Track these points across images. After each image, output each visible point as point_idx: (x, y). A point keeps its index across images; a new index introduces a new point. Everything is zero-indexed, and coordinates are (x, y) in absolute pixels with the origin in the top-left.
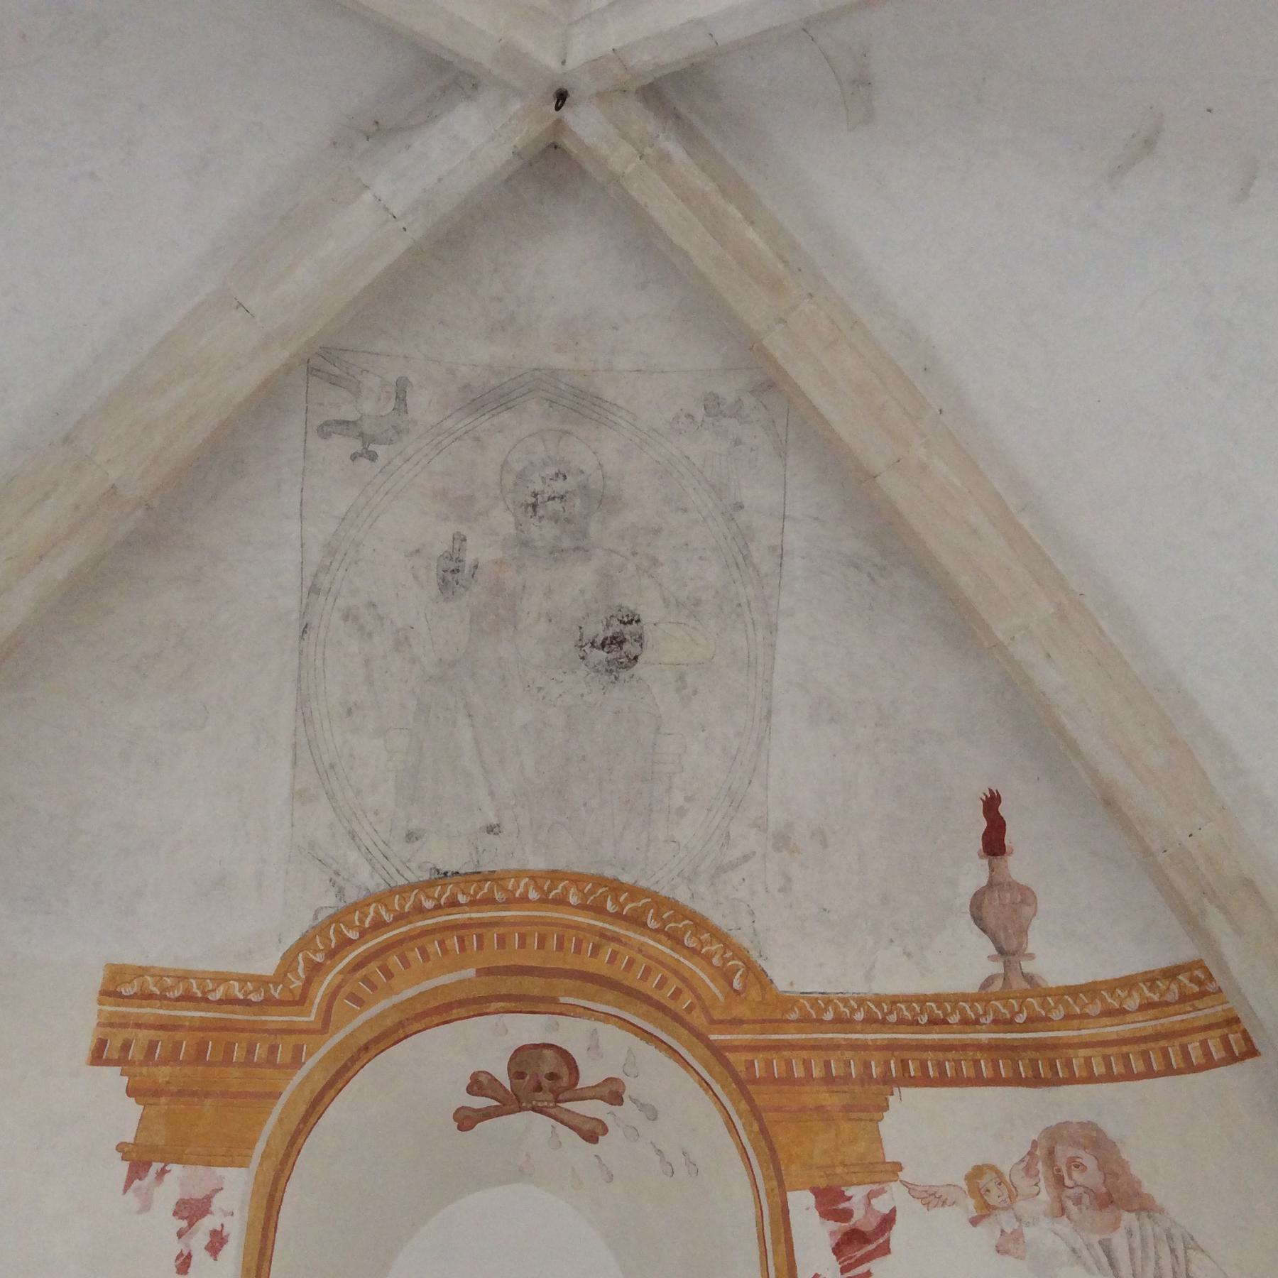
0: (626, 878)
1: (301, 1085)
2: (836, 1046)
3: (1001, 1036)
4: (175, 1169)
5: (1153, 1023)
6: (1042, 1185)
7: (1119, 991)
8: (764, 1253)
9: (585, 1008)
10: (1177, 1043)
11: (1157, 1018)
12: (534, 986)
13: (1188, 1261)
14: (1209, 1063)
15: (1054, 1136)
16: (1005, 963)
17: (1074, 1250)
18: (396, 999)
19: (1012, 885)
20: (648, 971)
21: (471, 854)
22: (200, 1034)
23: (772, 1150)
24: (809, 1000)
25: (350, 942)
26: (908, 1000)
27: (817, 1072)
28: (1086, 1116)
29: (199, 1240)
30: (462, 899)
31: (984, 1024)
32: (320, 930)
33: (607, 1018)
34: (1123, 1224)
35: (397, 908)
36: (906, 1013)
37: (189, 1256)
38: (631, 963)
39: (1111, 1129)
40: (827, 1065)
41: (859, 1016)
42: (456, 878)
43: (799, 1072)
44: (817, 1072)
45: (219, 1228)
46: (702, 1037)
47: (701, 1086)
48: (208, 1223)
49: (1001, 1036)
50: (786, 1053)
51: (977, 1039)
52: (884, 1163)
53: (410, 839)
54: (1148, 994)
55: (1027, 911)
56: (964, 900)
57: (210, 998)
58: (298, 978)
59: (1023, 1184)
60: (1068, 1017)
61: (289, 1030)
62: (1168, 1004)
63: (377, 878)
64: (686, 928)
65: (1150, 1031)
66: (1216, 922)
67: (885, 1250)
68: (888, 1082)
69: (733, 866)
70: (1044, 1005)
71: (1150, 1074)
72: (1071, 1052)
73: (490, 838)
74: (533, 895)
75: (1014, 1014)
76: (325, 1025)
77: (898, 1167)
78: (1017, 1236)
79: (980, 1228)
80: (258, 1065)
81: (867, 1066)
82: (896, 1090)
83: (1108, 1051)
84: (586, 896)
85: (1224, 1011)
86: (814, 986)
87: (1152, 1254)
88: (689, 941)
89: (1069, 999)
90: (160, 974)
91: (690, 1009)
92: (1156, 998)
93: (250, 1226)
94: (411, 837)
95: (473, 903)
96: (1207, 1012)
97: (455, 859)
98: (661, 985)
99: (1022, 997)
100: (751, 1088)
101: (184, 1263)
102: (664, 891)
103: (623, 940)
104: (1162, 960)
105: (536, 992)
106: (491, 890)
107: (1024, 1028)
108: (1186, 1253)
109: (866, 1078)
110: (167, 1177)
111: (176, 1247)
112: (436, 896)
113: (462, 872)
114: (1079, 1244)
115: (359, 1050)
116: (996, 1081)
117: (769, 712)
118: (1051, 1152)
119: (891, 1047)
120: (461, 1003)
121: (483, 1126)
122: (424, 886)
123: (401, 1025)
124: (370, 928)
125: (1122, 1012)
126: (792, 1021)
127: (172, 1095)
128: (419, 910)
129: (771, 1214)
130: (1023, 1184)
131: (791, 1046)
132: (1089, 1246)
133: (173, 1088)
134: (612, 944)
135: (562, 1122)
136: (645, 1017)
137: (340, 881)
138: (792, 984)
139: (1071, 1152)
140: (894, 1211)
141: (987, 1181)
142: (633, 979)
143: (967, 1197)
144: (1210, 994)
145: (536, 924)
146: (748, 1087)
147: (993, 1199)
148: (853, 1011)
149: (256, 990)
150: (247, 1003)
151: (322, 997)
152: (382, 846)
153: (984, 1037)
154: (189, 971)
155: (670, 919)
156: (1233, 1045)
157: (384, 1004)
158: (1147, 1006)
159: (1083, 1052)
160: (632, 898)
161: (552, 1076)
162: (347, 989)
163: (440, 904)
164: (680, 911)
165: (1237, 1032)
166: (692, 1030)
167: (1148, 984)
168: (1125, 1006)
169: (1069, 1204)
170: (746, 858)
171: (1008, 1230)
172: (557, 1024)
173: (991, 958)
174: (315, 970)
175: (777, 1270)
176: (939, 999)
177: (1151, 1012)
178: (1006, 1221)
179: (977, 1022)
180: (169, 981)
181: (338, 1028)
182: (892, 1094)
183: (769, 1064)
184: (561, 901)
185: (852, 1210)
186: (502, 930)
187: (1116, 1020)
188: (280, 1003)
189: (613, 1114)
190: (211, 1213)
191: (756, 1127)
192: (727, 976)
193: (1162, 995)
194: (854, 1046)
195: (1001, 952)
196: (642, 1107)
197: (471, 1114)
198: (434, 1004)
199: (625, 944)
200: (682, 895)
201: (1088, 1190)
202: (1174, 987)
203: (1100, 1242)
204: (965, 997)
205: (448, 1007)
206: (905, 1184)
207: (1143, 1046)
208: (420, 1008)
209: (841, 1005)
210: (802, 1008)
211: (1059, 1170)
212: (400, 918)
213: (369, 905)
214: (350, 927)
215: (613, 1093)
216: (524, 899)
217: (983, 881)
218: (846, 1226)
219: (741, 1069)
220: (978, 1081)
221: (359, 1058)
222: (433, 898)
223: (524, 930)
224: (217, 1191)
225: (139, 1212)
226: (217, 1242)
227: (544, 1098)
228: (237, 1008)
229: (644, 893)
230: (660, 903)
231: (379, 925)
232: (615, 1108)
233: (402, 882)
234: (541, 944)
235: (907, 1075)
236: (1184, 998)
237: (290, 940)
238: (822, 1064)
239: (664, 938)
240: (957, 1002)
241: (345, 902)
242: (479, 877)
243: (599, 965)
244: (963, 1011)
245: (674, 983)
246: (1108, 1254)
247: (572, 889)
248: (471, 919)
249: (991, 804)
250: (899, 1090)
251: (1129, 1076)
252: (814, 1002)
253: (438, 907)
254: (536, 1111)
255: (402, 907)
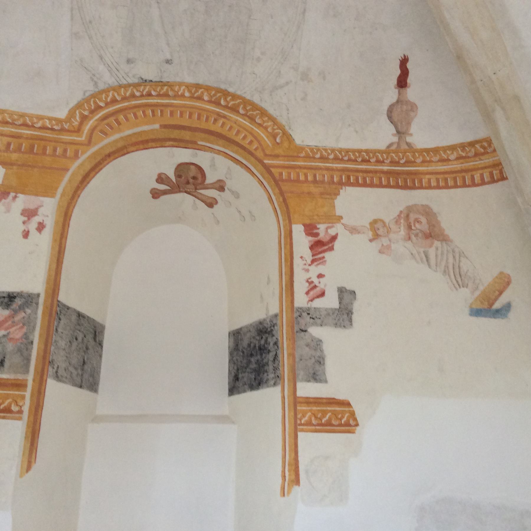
0: (231, 90)
1: (79, 167)
2: (320, 168)
3: (394, 168)
4: (21, 196)
5: (460, 165)
6: (402, 228)
7: (448, 152)
8: (280, 249)
9: (210, 147)
10: (470, 174)
11: (462, 163)
12: (187, 135)
13: (460, 261)
14: (483, 183)
15: (410, 209)
16: (399, 137)
17: (412, 254)
18: (122, 134)
19: (408, 102)
20: (238, 132)
21: (158, 73)
22: (31, 141)
23: (287, 208)
24: (310, 149)
25: (101, 107)
26: (354, 151)
27: (310, 178)
28: (425, 203)
29: (33, 226)
30: (153, 93)
31: (386, 163)
32: (87, 100)
33: (219, 152)
34: (435, 245)
35: (123, 94)
36: (352, 157)
37: (28, 232)
38: (231, 128)
39: (435, 209)
40: (315, 176)
41: (331, 157)
42: (151, 83)
43: (302, 178)
44: (310, 178)
45: (42, 221)
46: (261, 162)
47: (259, 183)
48: (36, 220)
49: (394, 168)
50: (298, 170)
51: (382, 169)
52: (335, 216)
53: (129, 62)
54: (461, 153)
55: (412, 114)
56: (385, 108)
57: (35, 126)
58: (76, 121)
59: (393, 227)
60: (424, 162)
61: (72, 143)
62: (469, 157)
63: (113, 80)
64: (257, 114)
65: (459, 169)
66: (499, 115)
67: (332, 249)
68: (341, 184)
69: (281, 87)
70: (414, 156)
71: (456, 186)
72: (422, 176)
73: (167, 66)
74: (187, 94)
75: (400, 159)
76: (89, 142)
77: (341, 218)
78: (389, 247)
79: (374, 243)
80: (58, 156)
81: (332, 177)
82: (344, 187)
83: (438, 176)
84: (211, 97)
85: (493, 160)
86: (312, 143)
87: (445, 258)
88: (258, 120)
89: (426, 154)
90: (11, 114)
91: (256, 149)
92: (464, 154)
93: (56, 223)
94: (129, 61)
95: (159, 95)
96: (487, 160)
97: (151, 74)
98: (245, 138)
99: (405, 152)
100: (280, 183)
101: (26, 234)
102: (248, 97)
103: (228, 117)
104: (470, 138)
105: (188, 138)
106: (167, 90)
107: (404, 165)
108: (459, 258)
109: (332, 182)
110: (17, 199)
111: (22, 228)
112: (141, 90)
113: (154, 80)
114: (415, 252)
115: (106, 156)
116: (388, 186)
117: (305, 10)
118: (408, 216)
119: (344, 170)
120: (154, 140)
121: (164, 198)
122: (136, 85)
123: (125, 147)
124: (110, 102)
125: (448, 160)
126: (301, 157)
127: (19, 165)
128: (133, 96)
129: (285, 234)
130: (393, 227)
131: (300, 167)
132: (419, 253)
133: (19, 163)
134: (223, 119)
135: (199, 199)
136: (236, 152)
137: (95, 79)
138: (303, 142)
139: (417, 216)
140: (337, 234)
141: (379, 225)
142: (232, 135)
143: (369, 230)
144: (488, 153)
145: (188, 107)
146: (279, 182)
147: (380, 232)
148: (329, 154)
149: (57, 124)
150: (52, 129)
151: (89, 130)
152: (115, 64)
153: (385, 168)
154: (26, 114)
155: (250, 110)
156: (495, 175)
157: (116, 136)
158: (459, 158)
159: (428, 176)
160: (232, 100)
161: (194, 178)
162: (99, 128)
163: (143, 94)
164: (255, 107)
165: (497, 170)
166: (256, 158)
167: (462, 148)
168: (450, 158)
169: (413, 237)
170: (287, 83)
171: (385, 244)
172: (196, 154)
173: (394, 135)
174: (84, 118)
175: (285, 254)
176: (367, 151)
177: (461, 161)
178: (385, 241)
179: (383, 162)
180: (16, 117)
181: (95, 144)
182: (342, 189)
183: (289, 174)
184: (200, 98)
185: (319, 233)
186: (172, 109)
187: (445, 163)
188: (68, 131)
189: (220, 196)
190: (38, 215)
191: (281, 199)
192: (274, 136)
193: (467, 153)
194: (328, 169)
195: (398, 132)
196: (233, 192)
197: (157, 192)
198: (140, 139)
199: (228, 120)
200: (256, 99)
201: (421, 231)
202: (473, 150)
203: (424, 252)
204: (379, 151)
205: (147, 141)
206: (343, 224)
207: (454, 175)
208: (134, 140)
209: (324, 152)
210: (306, 152)
211: (410, 223)
212: (124, 99)
213: (109, 91)
214: (101, 100)
215: (220, 186)
216: (183, 96)
217: (394, 100)
218: (316, 239)
219: (277, 175)
220: (381, 186)
221: (106, 160)
222: (140, 91)
223: (183, 109)
224: (40, 206)
225: (5, 212)
226: (41, 227)
227: (191, 187)
228: (48, 131)
229: (239, 97)
230: (246, 102)
231: (114, 101)
232: (221, 193)
233: (125, 82)
234: (190, 117)
235: (349, 182)
236: (476, 155)
237: (73, 103)
238: (313, 175)
239: (247, 118)
240: (375, 153)
241: (98, 89)
242: (161, 84)
243: (217, 128)
244: (377, 157)
245: (250, 138)
246: (427, 257)
247: (205, 93)
248: (158, 103)
249: (404, 62)
250: (345, 188)
251: (447, 187)
252: (312, 150)
253: (142, 96)
254: (187, 193)
255: (125, 94)
